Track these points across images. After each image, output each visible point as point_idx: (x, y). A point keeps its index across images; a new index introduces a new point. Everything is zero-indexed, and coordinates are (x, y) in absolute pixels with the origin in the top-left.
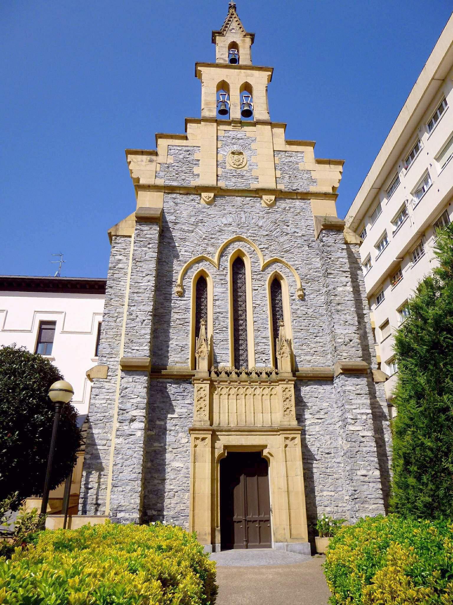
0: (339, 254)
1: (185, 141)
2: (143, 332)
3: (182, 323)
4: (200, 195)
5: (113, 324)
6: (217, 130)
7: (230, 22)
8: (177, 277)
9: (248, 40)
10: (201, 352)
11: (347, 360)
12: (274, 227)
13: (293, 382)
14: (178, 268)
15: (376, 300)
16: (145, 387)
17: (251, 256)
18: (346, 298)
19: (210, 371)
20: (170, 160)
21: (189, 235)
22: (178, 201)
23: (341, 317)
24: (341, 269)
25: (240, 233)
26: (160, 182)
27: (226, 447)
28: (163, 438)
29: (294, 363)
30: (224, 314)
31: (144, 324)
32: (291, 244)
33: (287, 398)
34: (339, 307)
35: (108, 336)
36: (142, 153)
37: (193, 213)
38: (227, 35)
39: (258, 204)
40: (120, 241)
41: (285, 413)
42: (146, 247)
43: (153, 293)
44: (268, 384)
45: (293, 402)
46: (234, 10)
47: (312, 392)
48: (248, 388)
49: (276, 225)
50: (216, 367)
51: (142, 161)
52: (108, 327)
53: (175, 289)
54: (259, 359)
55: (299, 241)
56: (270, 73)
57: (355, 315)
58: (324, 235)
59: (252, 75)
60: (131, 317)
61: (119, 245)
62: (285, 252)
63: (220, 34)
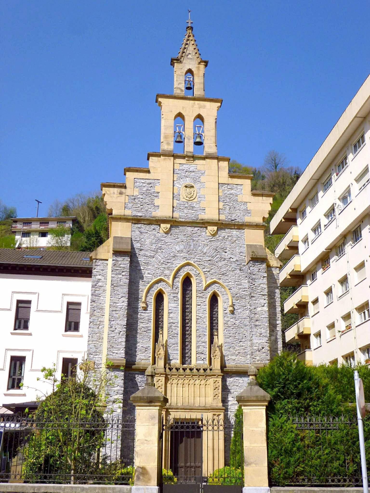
0: (261, 281)
1: (148, 174)
2: (120, 340)
3: (146, 330)
4: (160, 225)
5: (96, 330)
6: (174, 163)
7: (187, 46)
8: (142, 295)
9: (202, 66)
10: (160, 354)
11: (259, 362)
12: (215, 254)
13: (221, 377)
14: (143, 287)
15: (312, 276)
16: (123, 380)
17: (197, 278)
18: (263, 316)
19: (165, 368)
20: (136, 193)
21: (151, 260)
22: (142, 230)
23: (258, 331)
24: (262, 293)
25: (189, 259)
26: (128, 213)
27: (174, 419)
28: (133, 412)
29: (224, 361)
30: (176, 324)
31: (120, 335)
32: (227, 268)
33: (217, 388)
34: (257, 323)
35: (93, 339)
36: (114, 186)
37: (154, 241)
38: (184, 61)
39: (204, 233)
40: (99, 264)
41: (215, 397)
42: (120, 274)
43: (127, 311)
44: (204, 377)
45: (220, 390)
46: (190, 31)
47: (235, 382)
48: (190, 380)
49: (217, 252)
50: (169, 364)
51: (114, 193)
52: (93, 332)
53: (141, 305)
54: (199, 358)
55: (233, 265)
56: (219, 104)
57: (268, 329)
58: (251, 265)
59: (204, 107)
60: (112, 329)
61: (98, 267)
62: (223, 274)
63: (178, 60)
